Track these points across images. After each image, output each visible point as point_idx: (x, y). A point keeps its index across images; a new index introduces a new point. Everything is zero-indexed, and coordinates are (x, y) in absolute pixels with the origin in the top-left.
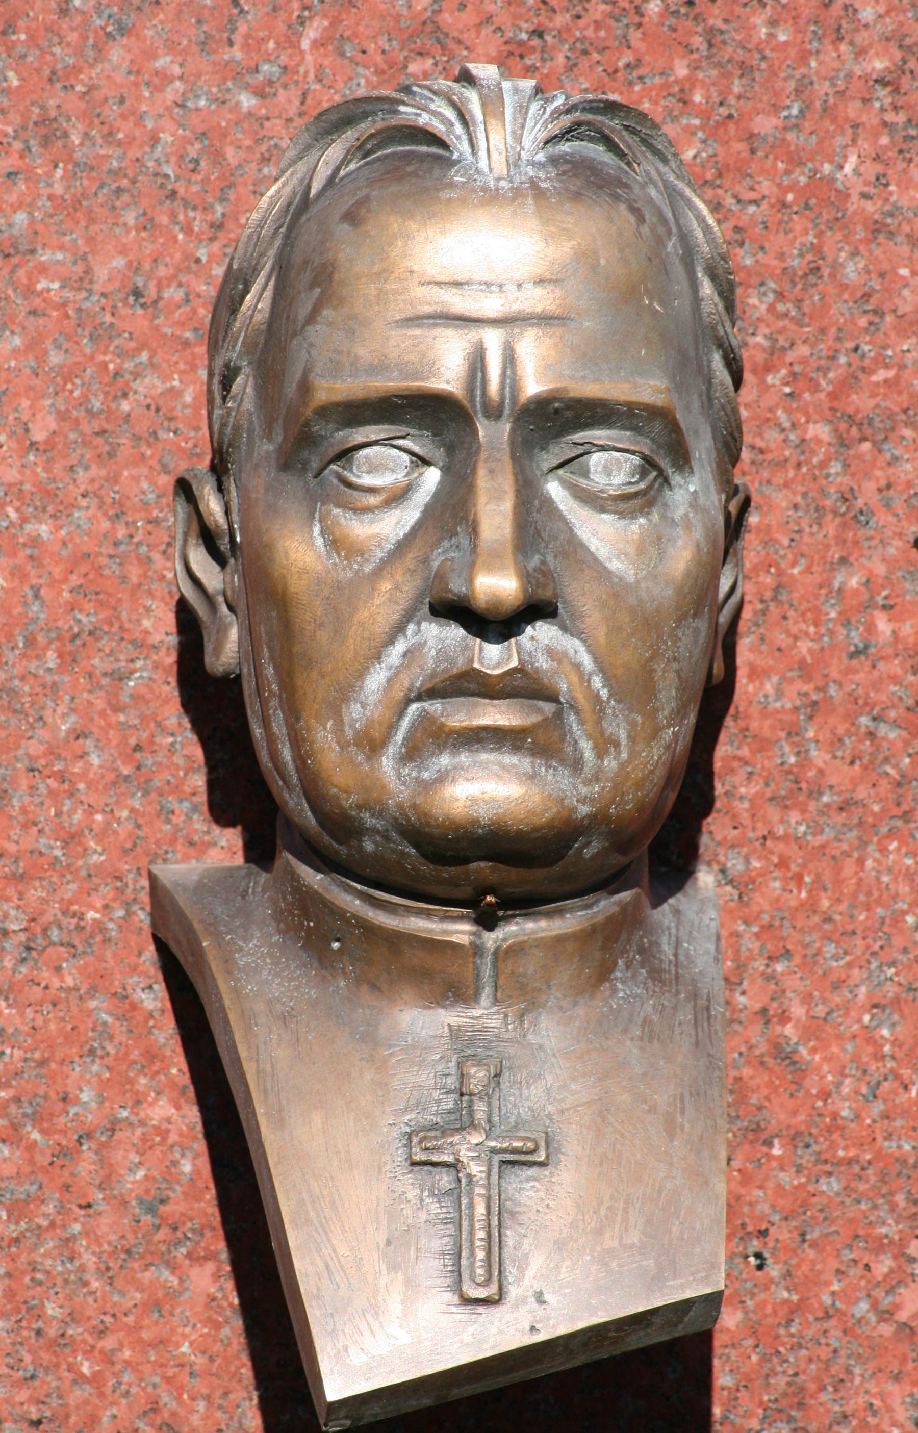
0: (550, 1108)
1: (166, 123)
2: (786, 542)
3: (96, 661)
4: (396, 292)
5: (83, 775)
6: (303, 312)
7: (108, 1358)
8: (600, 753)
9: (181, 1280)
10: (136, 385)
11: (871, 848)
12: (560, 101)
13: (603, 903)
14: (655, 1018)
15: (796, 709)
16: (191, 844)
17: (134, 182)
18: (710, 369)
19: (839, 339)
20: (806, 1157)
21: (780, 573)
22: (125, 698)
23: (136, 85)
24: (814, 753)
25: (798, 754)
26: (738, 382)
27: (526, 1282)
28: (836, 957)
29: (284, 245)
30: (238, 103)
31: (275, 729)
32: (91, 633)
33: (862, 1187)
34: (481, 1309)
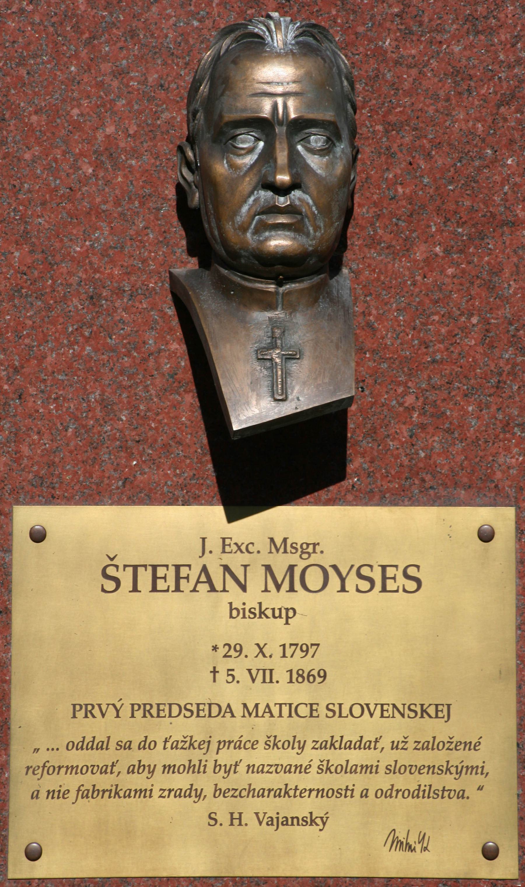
0: (300, 342)
1: (170, 31)
2: (369, 163)
3: (151, 204)
4: (249, 86)
5: (147, 241)
6: (219, 92)
7: (160, 422)
8: (315, 231)
9: (182, 398)
10: (162, 115)
11: (397, 260)
12: (298, 24)
13: (315, 278)
14: (332, 314)
15: (373, 217)
16: (182, 262)
17: (160, 50)
18: (347, 109)
19: (385, 98)
20: (377, 357)
21: (368, 173)
22: (160, 216)
23: (160, 18)
24: (379, 231)
25: (374, 231)
26: (355, 113)
27: (294, 394)
28: (386, 295)
29: (212, 71)
30: (193, 24)
31: (213, 225)
32: (149, 195)
33: (394, 366)
34: (280, 403)
